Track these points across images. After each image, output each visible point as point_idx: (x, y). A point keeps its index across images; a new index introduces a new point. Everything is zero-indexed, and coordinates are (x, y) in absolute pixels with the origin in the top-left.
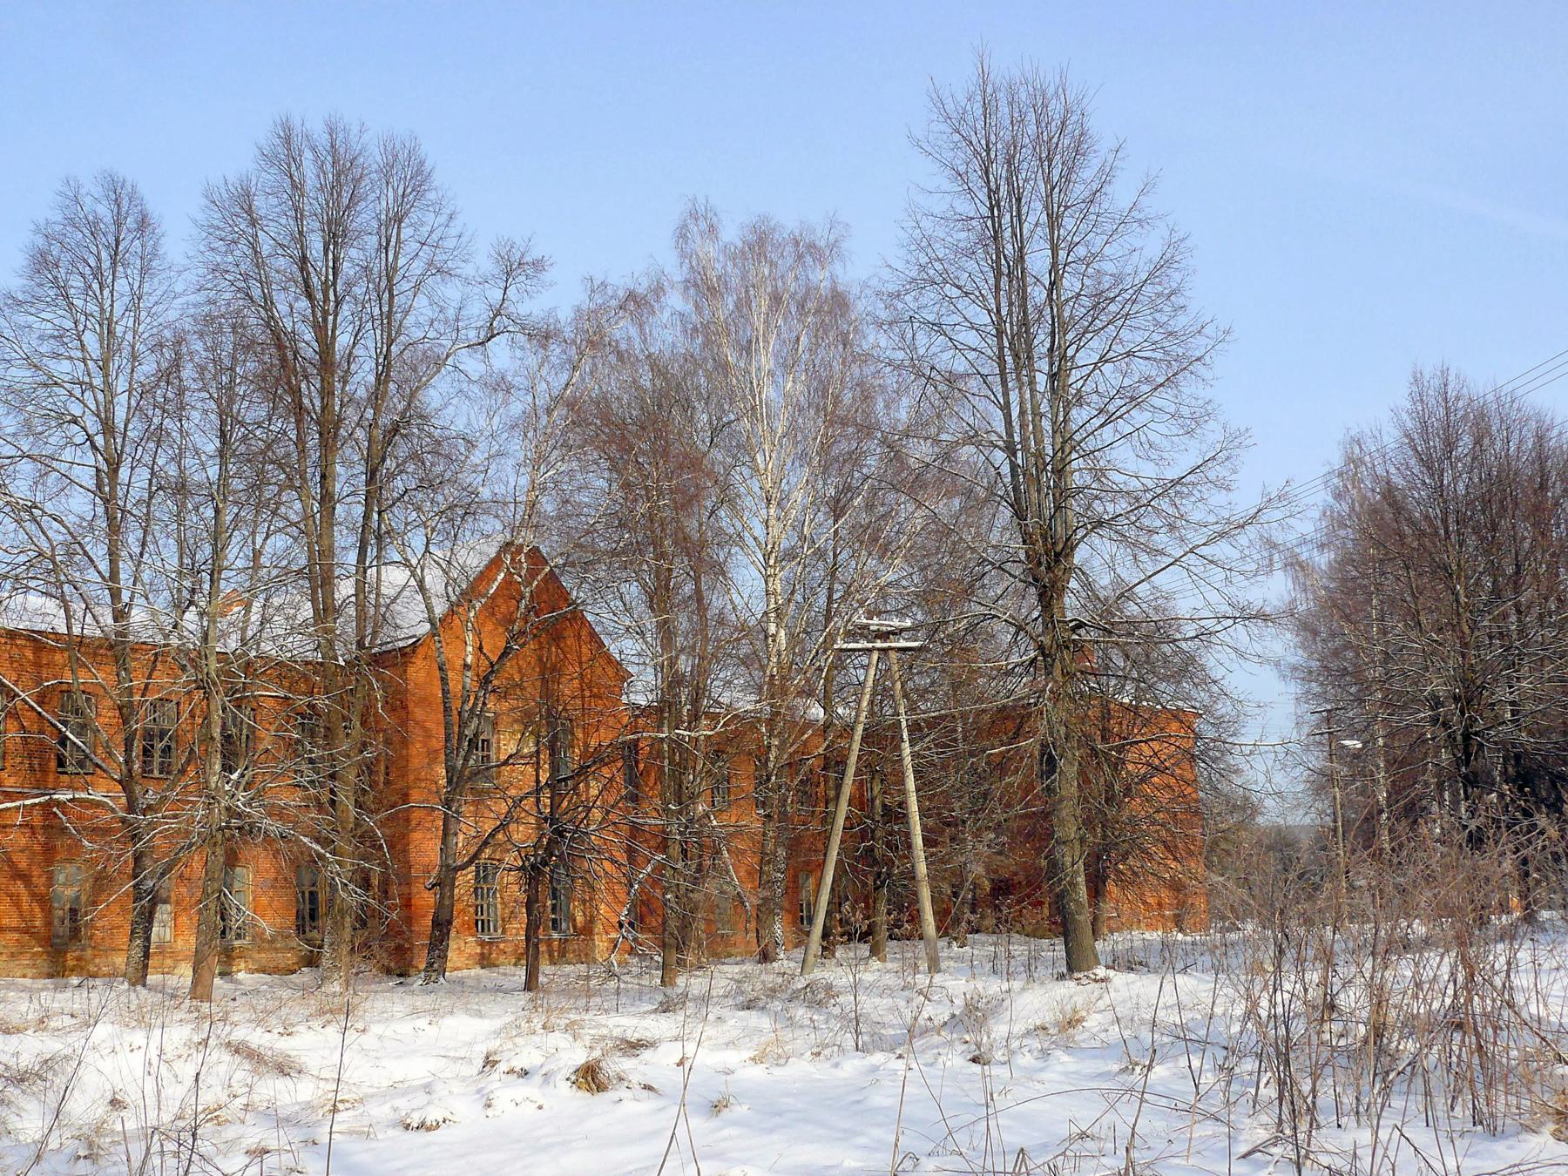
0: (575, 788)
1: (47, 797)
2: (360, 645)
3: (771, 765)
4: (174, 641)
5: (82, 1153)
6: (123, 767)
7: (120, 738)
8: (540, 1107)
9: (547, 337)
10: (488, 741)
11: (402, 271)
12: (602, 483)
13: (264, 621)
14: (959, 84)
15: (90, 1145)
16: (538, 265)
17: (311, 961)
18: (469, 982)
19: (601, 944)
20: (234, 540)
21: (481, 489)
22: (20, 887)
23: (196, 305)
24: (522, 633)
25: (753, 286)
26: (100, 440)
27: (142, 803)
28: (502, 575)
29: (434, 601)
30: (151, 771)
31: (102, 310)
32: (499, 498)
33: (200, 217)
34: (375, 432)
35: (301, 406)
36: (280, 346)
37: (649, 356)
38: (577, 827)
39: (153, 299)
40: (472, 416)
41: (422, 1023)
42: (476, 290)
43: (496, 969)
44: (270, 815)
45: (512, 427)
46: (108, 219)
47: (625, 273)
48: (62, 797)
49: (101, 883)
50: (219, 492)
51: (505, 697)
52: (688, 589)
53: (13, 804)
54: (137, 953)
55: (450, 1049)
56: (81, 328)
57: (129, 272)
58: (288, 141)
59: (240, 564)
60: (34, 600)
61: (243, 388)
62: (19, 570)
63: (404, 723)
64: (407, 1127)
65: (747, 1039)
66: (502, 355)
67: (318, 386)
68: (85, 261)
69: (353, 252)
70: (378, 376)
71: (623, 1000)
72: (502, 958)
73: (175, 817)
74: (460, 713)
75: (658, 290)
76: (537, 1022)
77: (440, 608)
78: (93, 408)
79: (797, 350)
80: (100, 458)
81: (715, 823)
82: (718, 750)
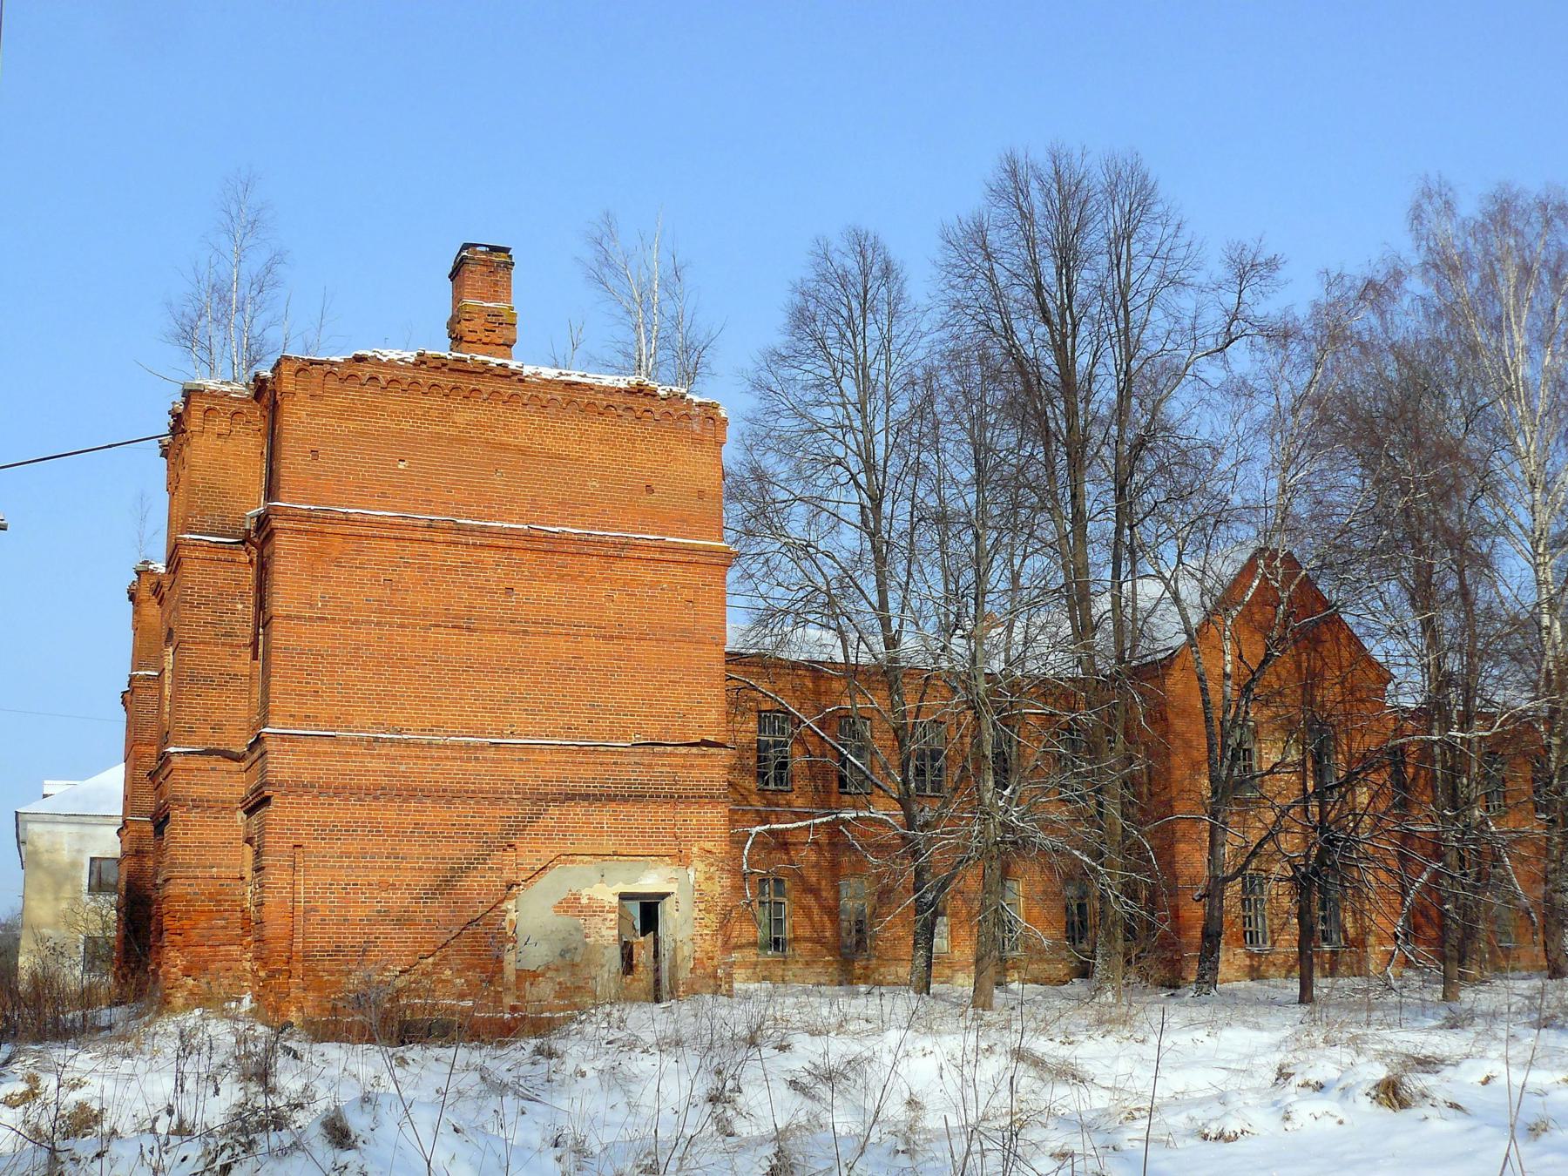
0: (1343, 796)
1: (834, 816)
2: (1120, 659)
3: (1553, 766)
4: (945, 665)
5: (901, 1147)
6: (901, 786)
7: (895, 760)
8: (1341, 1122)
9: (1286, 336)
10: (1249, 750)
11: (1135, 286)
12: (1355, 481)
13: (1027, 642)
15: (907, 1142)
16: (1272, 264)
17: (1084, 972)
18: (1240, 994)
19: (1375, 953)
20: (995, 564)
21: (1230, 496)
22: (810, 900)
23: (942, 342)
24: (1282, 639)
25: (1498, 260)
26: (862, 478)
27: (920, 821)
28: (1257, 581)
29: (1190, 612)
30: (925, 790)
31: (857, 357)
32: (1251, 503)
33: (939, 258)
34: (1120, 448)
35: (1047, 429)
36: (1024, 373)
37: (1392, 346)
38: (1349, 834)
39: (901, 341)
40: (1216, 423)
41: (1200, 1034)
42: (1211, 297)
43: (1266, 982)
44: (1043, 829)
45: (1257, 432)
46: (856, 271)
47: (1360, 263)
48: (847, 816)
49: (885, 895)
50: (977, 522)
51: (1267, 705)
52: (1452, 584)
53: (805, 823)
54: (921, 962)
55: (1231, 1061)
56: (838, 375)
57: (878, 317)
58: (1014, 174)
59: (1002, 586)
60: (813, 632)
61: (994, 416)
62: (797, 606)
63: (1165, 735)
64: (1205, 1137)
65: (1547, 1060)
66: (1242, 358)
67: (1062, 408)
68: (838, 312)
69: (1085, 274)
70: (1120, 393)
71: (1406, 1015)
72: (1272, 970)
73: (951, 832)
74: (1221, 723)
75: (1397, 276)
76: (1318, 1036)
77: (1195, 619)
78: (855, 449)
79: (1553, 321)
80: (864, 495)
81: (1493, 829)
82: (1493, 751)
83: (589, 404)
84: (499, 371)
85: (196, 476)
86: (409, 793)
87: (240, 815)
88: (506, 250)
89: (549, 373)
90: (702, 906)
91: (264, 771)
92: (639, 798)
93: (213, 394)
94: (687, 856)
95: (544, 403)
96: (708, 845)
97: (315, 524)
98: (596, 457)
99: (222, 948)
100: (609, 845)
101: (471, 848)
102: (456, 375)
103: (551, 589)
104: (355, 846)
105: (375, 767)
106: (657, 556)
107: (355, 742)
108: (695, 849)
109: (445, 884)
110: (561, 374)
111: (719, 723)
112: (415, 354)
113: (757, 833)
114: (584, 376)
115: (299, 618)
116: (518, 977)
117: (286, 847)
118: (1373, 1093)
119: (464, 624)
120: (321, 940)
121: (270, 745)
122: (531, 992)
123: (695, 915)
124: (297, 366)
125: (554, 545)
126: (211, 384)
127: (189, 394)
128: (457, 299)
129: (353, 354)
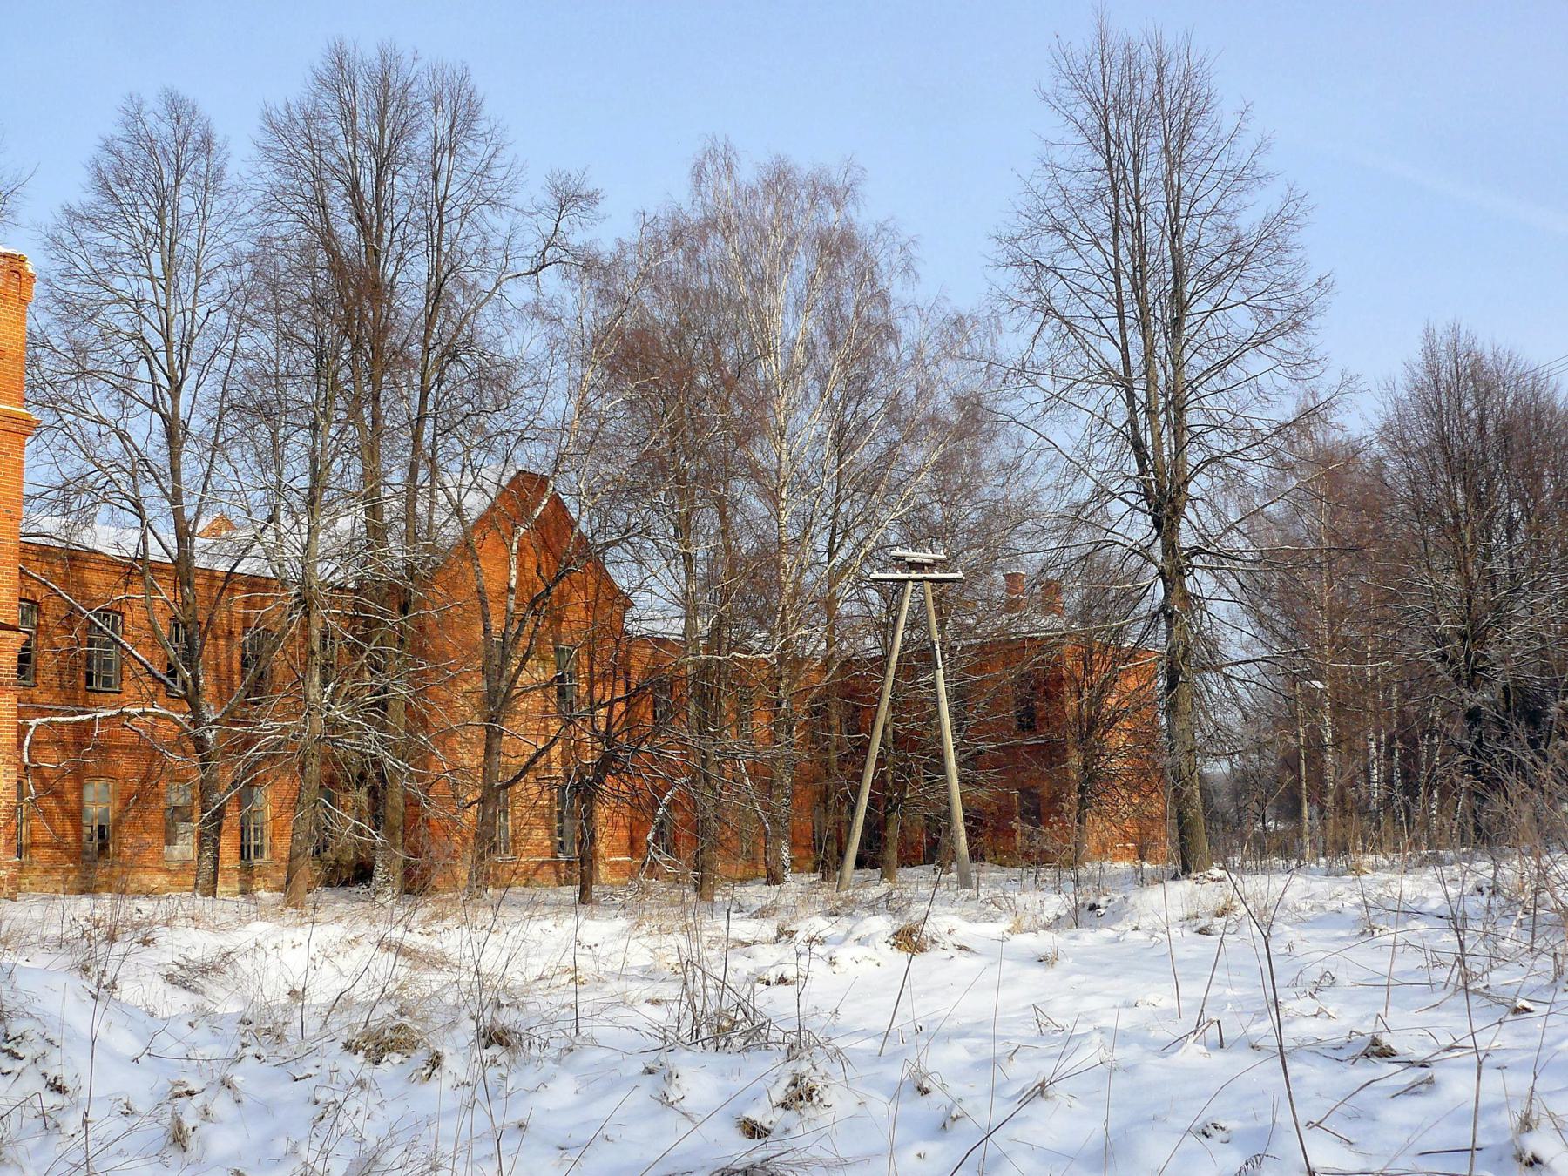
14: (1082, 42)
16: (592, 198)
78: (158, 326)
111: (10, 604)
113: (38, 725)
118: (892, 941)
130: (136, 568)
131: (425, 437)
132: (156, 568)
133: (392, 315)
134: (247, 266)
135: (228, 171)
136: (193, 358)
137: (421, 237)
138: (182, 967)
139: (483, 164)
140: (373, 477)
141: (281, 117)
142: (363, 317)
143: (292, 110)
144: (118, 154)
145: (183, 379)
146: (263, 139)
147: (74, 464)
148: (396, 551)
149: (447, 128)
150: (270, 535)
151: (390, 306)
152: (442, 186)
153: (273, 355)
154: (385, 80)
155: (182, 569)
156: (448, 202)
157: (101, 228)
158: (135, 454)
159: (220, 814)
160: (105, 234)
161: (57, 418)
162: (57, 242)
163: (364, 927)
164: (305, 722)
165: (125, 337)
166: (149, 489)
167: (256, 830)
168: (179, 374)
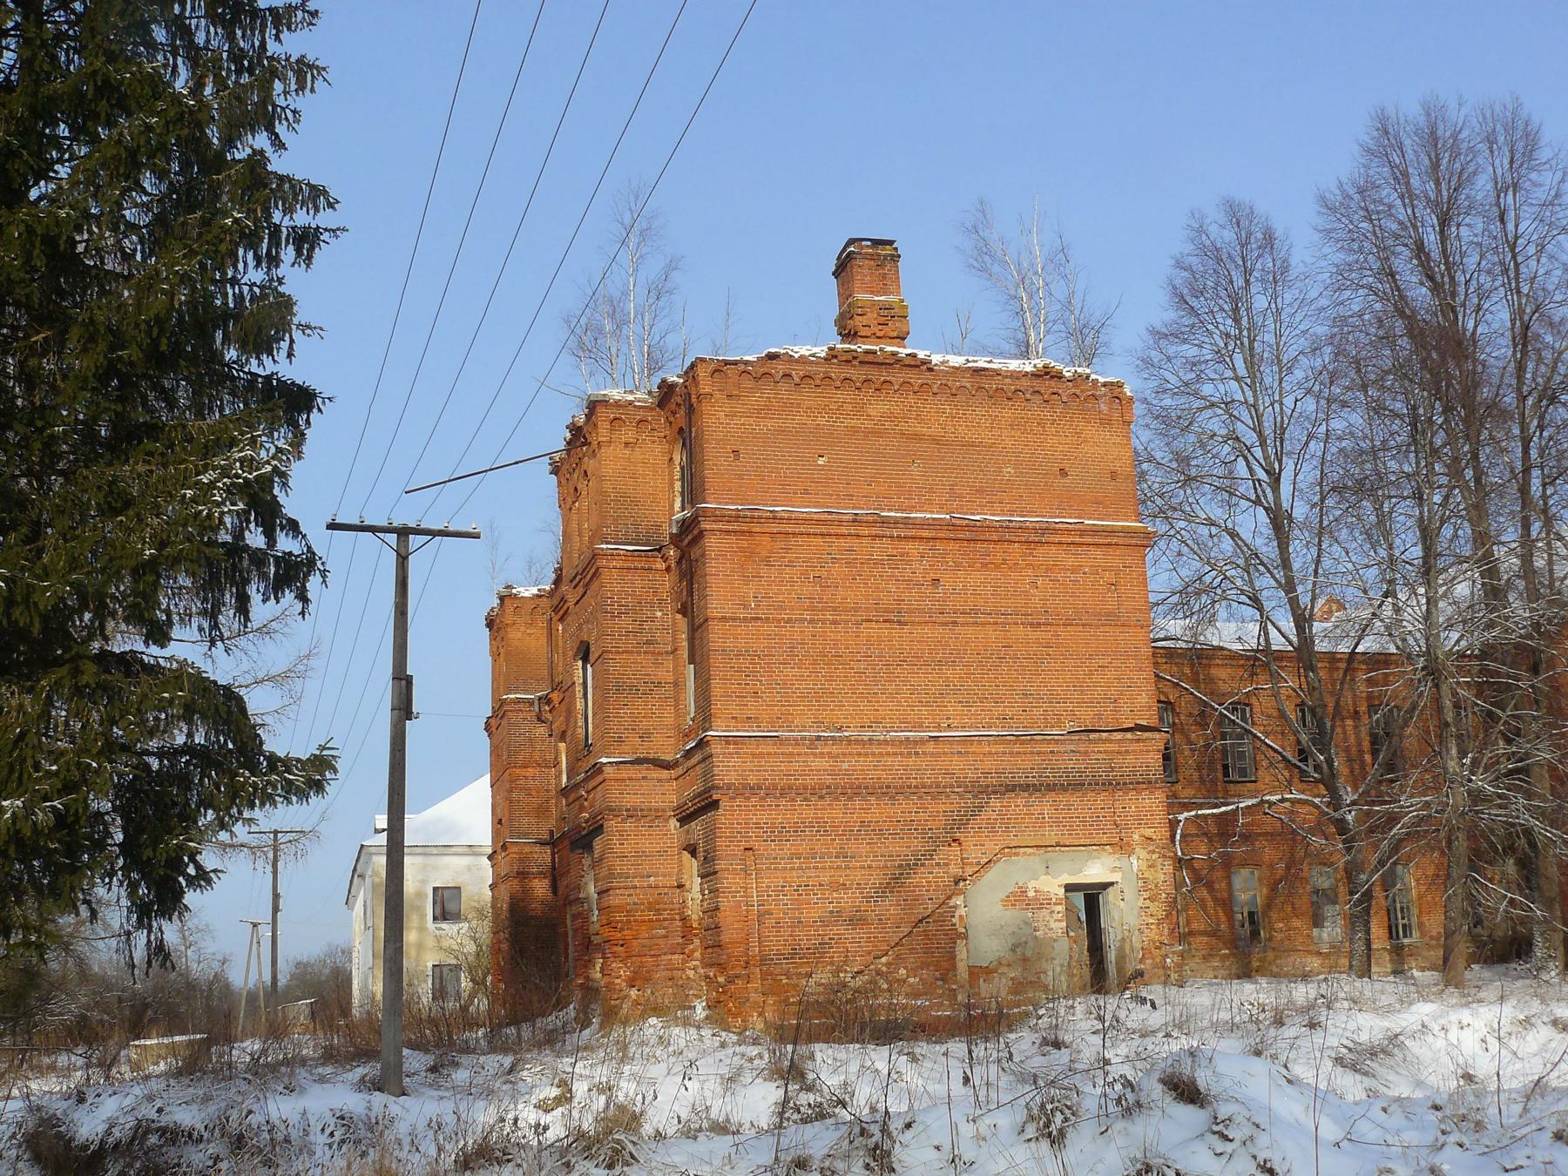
48: (1274, 798)
83: (997, 389)
84: (908, 361)
85: (608, 487)
86: (854, 791)
87: (673, 823)
88: (891, 243)
89: (956, 361)
90: (1146, 895)
91: (708, 775)
92: (1076, 786)
93: (617, 404)
94: (1129, 844)
95: (954, 391)
96: (1149, 832)
97: (743, 524)
98: (1009, 443)
99: (663, 957)
100: (1051, 836)
101: (917, 844)
102: (866, 367)
103: (977, 577)
104: (804, 847)
105: (818, 767)
106: (1078, 539)
107: (797, 742)
108: (1136, 837)
109: (896, 881)
110: (968, 361)
112: (825, 349)
114: (990, 362)
115: (734, 619)
116: (971, 974)
117: (738, 850)
119: (895, 618)
120: (776, 943)
121: (716, 749)
122: (985, 988)
123: (1140, 904)
124: (712, 367)
125: (974, 534)
126: (615, 394)
127: (593, 406)
128: (845, 294)
129: (766, 352)
130: (1260, 659)
131: (1534, 488)
132: (1280, 656)
133: (1479, 369)
134: (1328, 350)
135: (1294, 261)
136: (1288, 447)
137: (1497, 283)
138: (1350, 1050)
139: (1553, 193)
140: (1482, 539)
141: (1335, 197)
142: (1449, 377)
143: (1345, 187)
144: (1189, 269)
145: (1281, 470)
146: (1321, 222)
147: (1191, 568)
148: (1518, 609)
149: (1507, 166)
150: (1388, 611)
151: (1475, 360)
152: (1510, 227)
153: (1367, 431)
154: (1433, 133)
155: (1304, 653)
156: (1520, 241)
157: (1185, 341)
158: (1245, 549)
159: (1368, 895)
160: (1187, 346)
161: (1168, 527)
162: (1147, 363)
163: (1535, 1006)
164: (1448, 796)
165: (1220, 439)
166: (1264, 582)
167: (1402, 909)
168: (1276, 466)
